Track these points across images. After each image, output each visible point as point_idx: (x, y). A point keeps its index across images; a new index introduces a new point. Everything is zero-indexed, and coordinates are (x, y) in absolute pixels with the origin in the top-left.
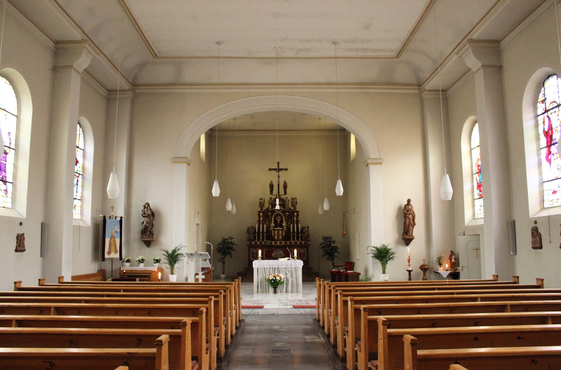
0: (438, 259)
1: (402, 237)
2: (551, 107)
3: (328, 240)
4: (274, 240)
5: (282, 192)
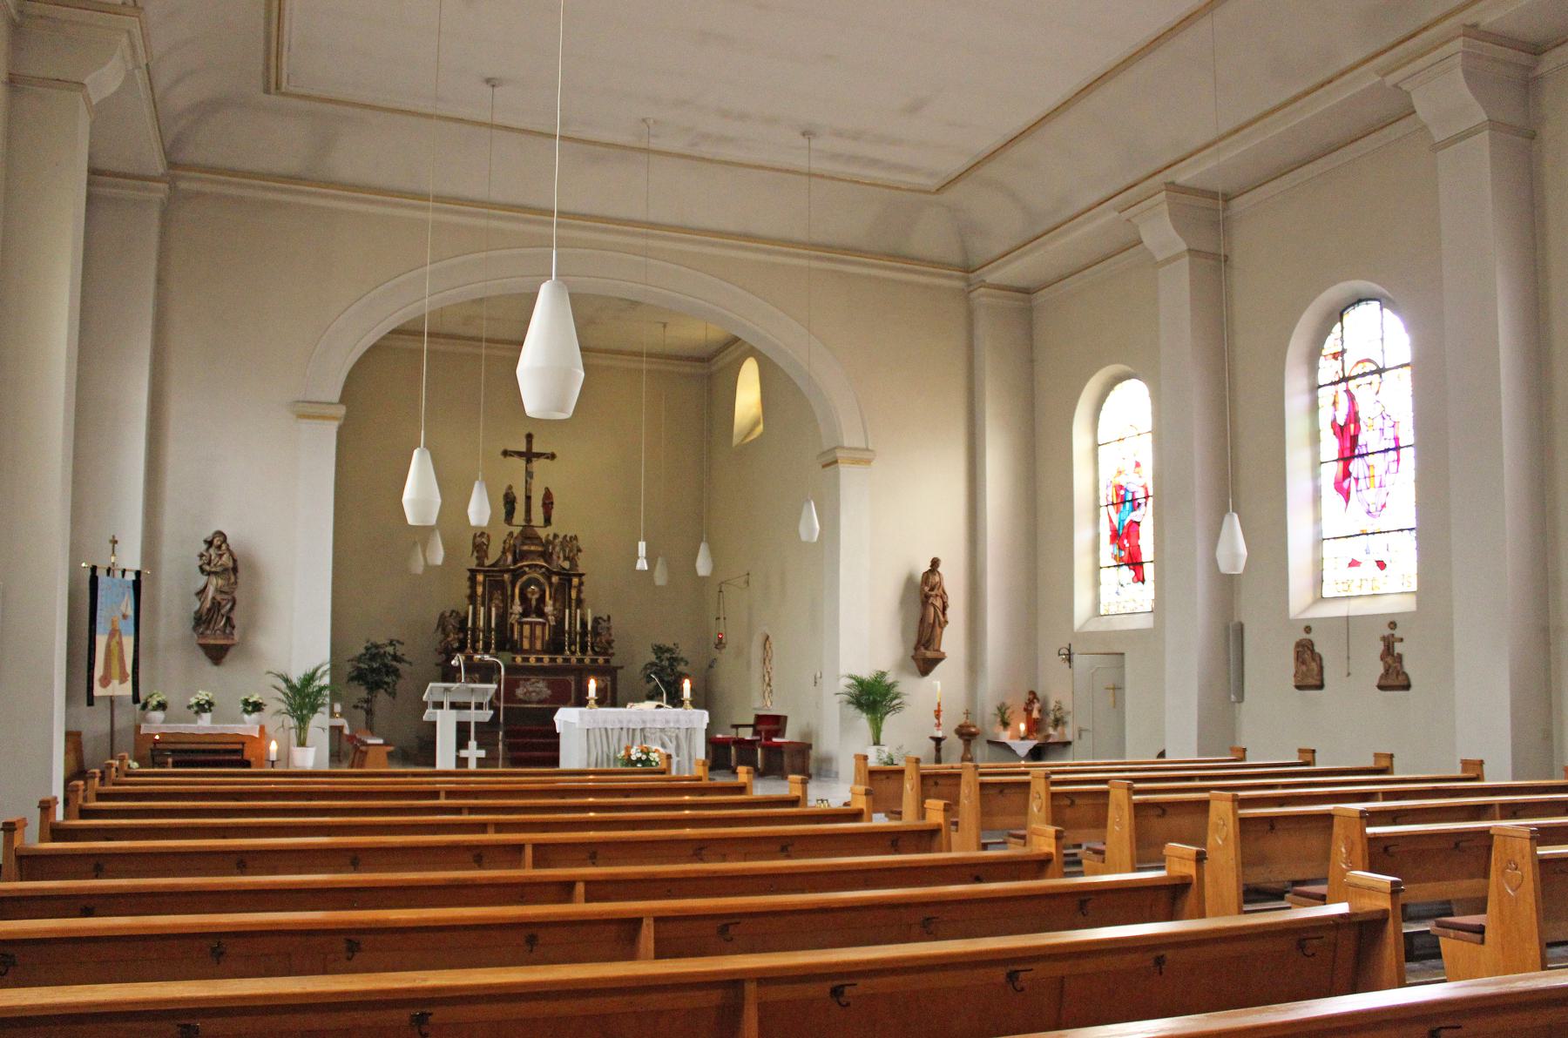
0: (999, 709)
1: (912, 652)
2: (1359, 370)
4: (521, 651)
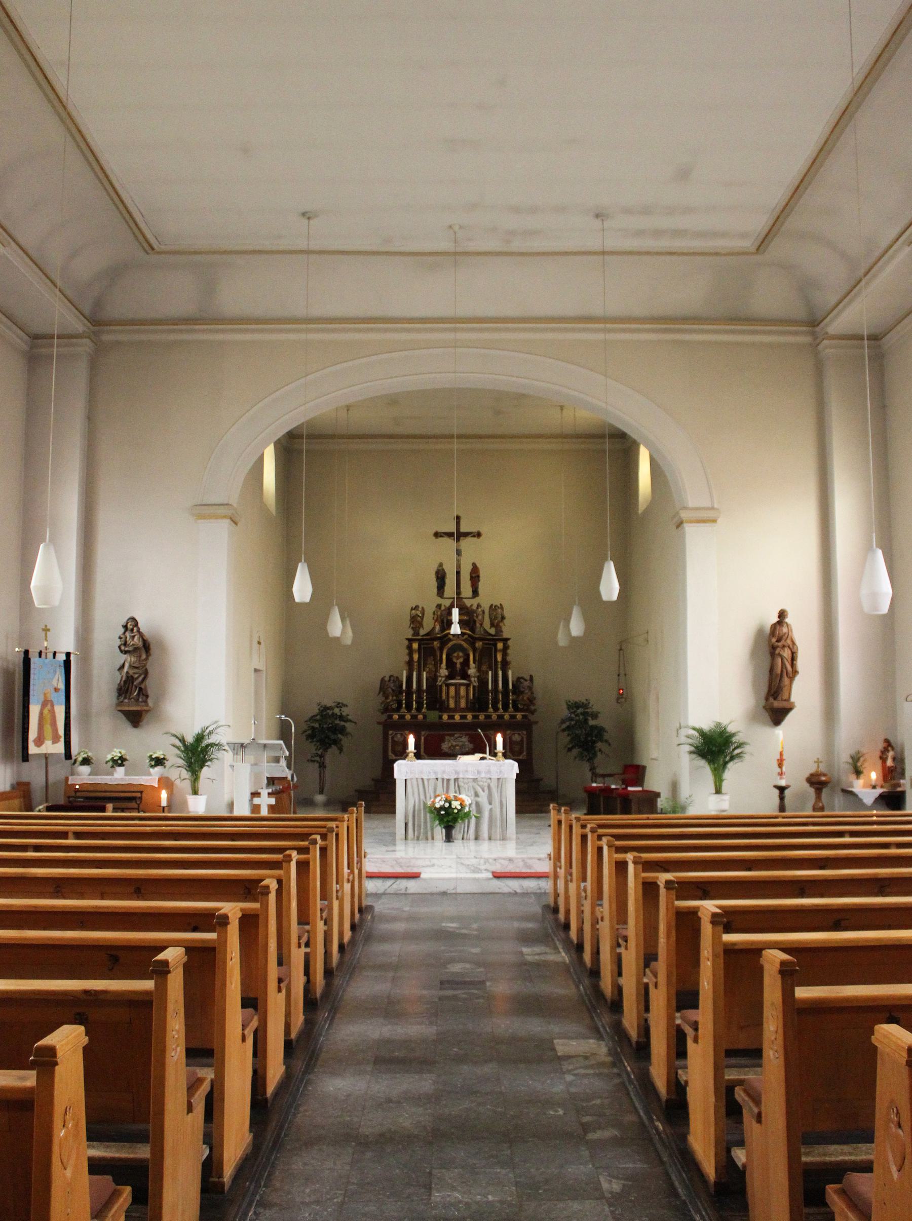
1: (763, 703)
3: (580, 710)
4: (446, 709)
5: (467, 590)
